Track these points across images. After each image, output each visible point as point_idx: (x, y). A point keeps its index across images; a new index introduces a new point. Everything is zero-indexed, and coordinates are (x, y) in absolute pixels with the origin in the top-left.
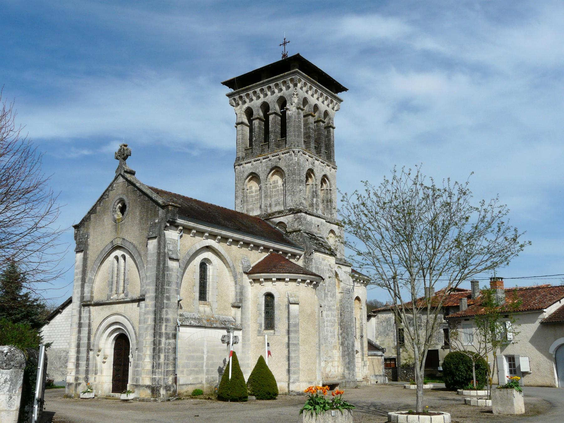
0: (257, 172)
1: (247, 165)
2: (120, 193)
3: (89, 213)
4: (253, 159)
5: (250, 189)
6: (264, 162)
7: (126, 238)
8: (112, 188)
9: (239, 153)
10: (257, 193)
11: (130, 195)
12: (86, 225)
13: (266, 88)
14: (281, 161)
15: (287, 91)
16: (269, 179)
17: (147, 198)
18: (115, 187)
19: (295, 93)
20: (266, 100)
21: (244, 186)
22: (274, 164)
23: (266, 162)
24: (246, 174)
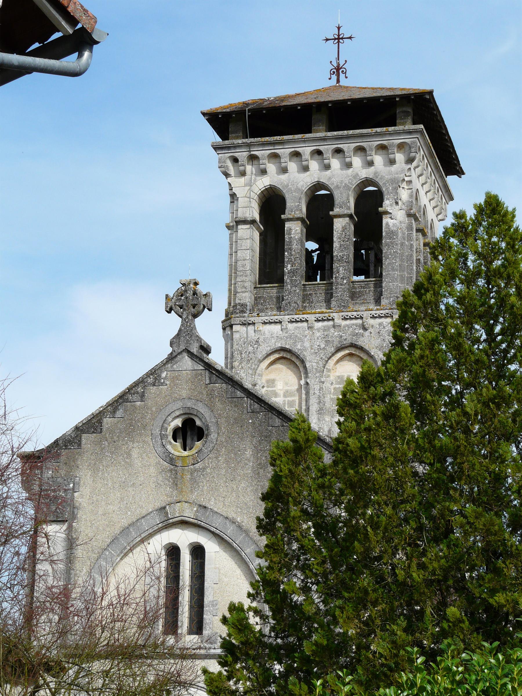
0: (297, 348)
1: (268, 327)
2: (184, 395)
3: (77, 428)
4: (287, 317)
5: (268, 387)
6: (318, 330)
7: (211, 505)
8: (156, 379)
9: (244, 295)
10: (290, 399)
11: (219, 405)
12: (63, 458)
13: (330, 152)
14: (367, 333)
15: (388, 168)
16: (329, 370)
17: (277, 421)
18: (165, 378)
19: (407, 179)
20: (324, 177)
21: (256, 377)
22: (348, 339)
23: (324, 330)
24: (264, 349)
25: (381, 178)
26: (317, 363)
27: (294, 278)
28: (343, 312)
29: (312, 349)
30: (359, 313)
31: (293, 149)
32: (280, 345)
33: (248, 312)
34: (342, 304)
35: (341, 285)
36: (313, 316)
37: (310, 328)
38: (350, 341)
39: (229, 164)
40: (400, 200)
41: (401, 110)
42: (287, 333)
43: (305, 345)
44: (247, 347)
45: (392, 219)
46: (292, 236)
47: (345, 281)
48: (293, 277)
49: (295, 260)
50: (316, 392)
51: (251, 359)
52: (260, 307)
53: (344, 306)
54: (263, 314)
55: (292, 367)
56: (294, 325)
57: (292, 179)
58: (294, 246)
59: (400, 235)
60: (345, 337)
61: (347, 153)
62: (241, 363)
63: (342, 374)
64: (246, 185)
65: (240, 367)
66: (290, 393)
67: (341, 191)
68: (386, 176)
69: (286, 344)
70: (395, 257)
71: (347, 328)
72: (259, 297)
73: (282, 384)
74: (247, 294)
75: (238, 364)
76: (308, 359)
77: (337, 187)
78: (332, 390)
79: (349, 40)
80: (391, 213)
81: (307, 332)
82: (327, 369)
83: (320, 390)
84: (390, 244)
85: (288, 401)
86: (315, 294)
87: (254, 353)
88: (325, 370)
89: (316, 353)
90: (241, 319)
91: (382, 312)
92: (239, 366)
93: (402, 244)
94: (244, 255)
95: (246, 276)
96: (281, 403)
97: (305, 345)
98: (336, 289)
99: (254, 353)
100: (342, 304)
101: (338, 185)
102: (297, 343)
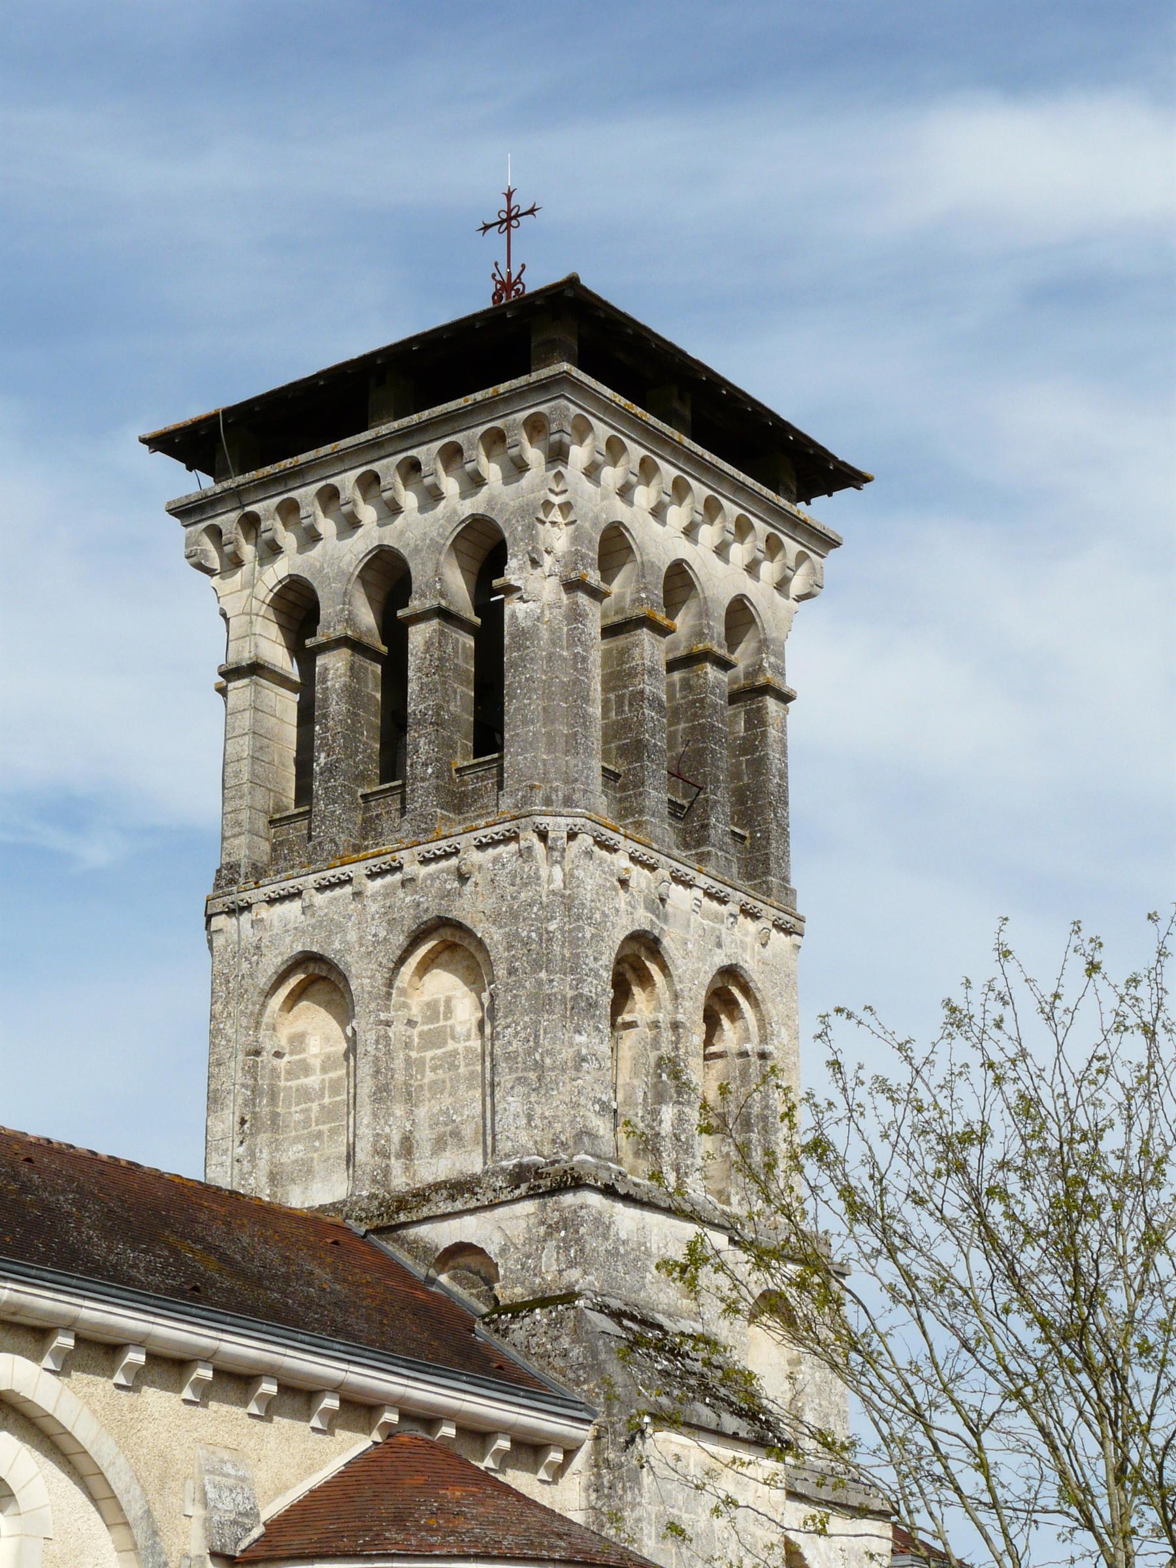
0: (332, 949)
1: (278, 908)
4: (312, 877)
5: (292, 1053)
6: (374, 897)
9: (236, 842)
14: (469, 888)
16: (403, 992)
20: (390, 536)
21: (262, 1033)
22: (432, 907)
24: (273, 962)
25: (501, 511)
26: (372, 977)
27: (332, 783)
28: (419, 844)
29: (361, 945)
30: (451, 841)
31: (323, 483)
32: (300, 949)
33: (242, 880)
34: (423, 826)
35: (423, 780)
36: (363, 864)
37: (357, 895)
38: (436, 913)
39: (208, 545)
40: (548, 552)
42: (313, 915)
43: (348, 937)
44: (239, 964)
45: (525, 602)
46: (329, 684)
47: (430, 771)
49: (334, 741)
50: (369, 1049)
51: (246, 991)
52: (282, 864)
53: (426, 831)
54: (266, 881)
56: (328, 894)
57: (329, 553)
58: (333, 708)
59: (545, 635)
60: (425, 906)
61: (426, 465)
62: (226, 1006)
63: (435, 996)
64: (243, 588)
66: (334, 1062)
67: (422, 559)
68: (512, 503)
69: (312, 943)
70: (529, 690)
72: (281, 843)
73: (318, 1043)
74: (242, 837)
75: (221, 1007)
76: (353, 971)
77: (417, 550)
78: (416, 1040)
79: (530, 216)
80: (518, 589)
81: (352, 907)
82: (398, 988)
83: (377, 1042)
84: (519, 662)
86: (387, 813)
87: (251, 975)
88: (394, 991)
89: (369, 953)
91: (496, 829)
93: (550, 658)
94: (239, 749)
95: (241, 798)
97: (348, 937)
98: (413, 791)
99: (251, 975)
100: (423, 826)
101: (417, 546)
102: (333, 938)
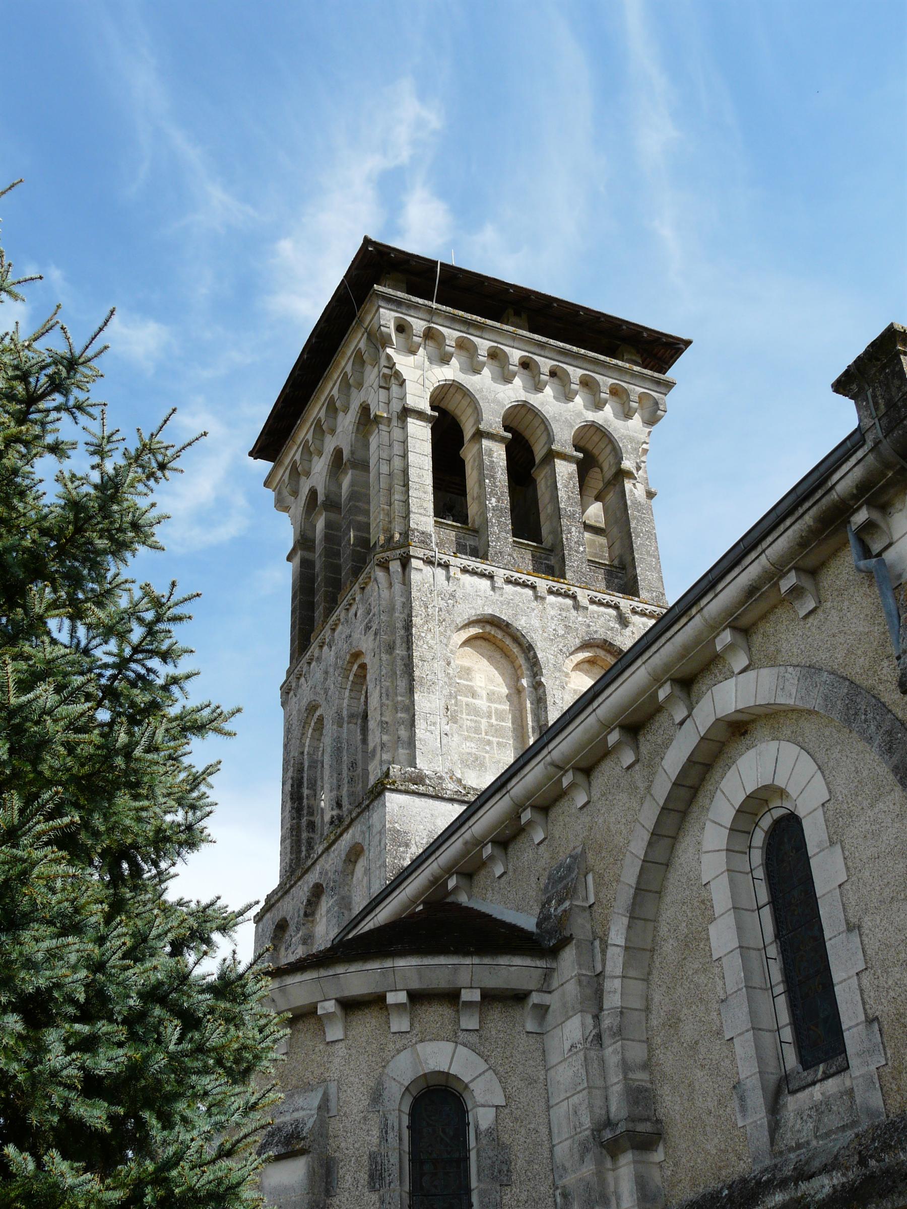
1: (467, 578)
4: (502, 571)
6: (552, 606)
32: (490, 612)
41: (629, 357)
48: (501, 517)
55: (498, 656)
65: (425, 628)
71: (596, 615)
75: (421, 622)
85: (496, 709)
90: (427, 552)
92: (423, 625)
96: (485, 709)
102: (520, 617)
